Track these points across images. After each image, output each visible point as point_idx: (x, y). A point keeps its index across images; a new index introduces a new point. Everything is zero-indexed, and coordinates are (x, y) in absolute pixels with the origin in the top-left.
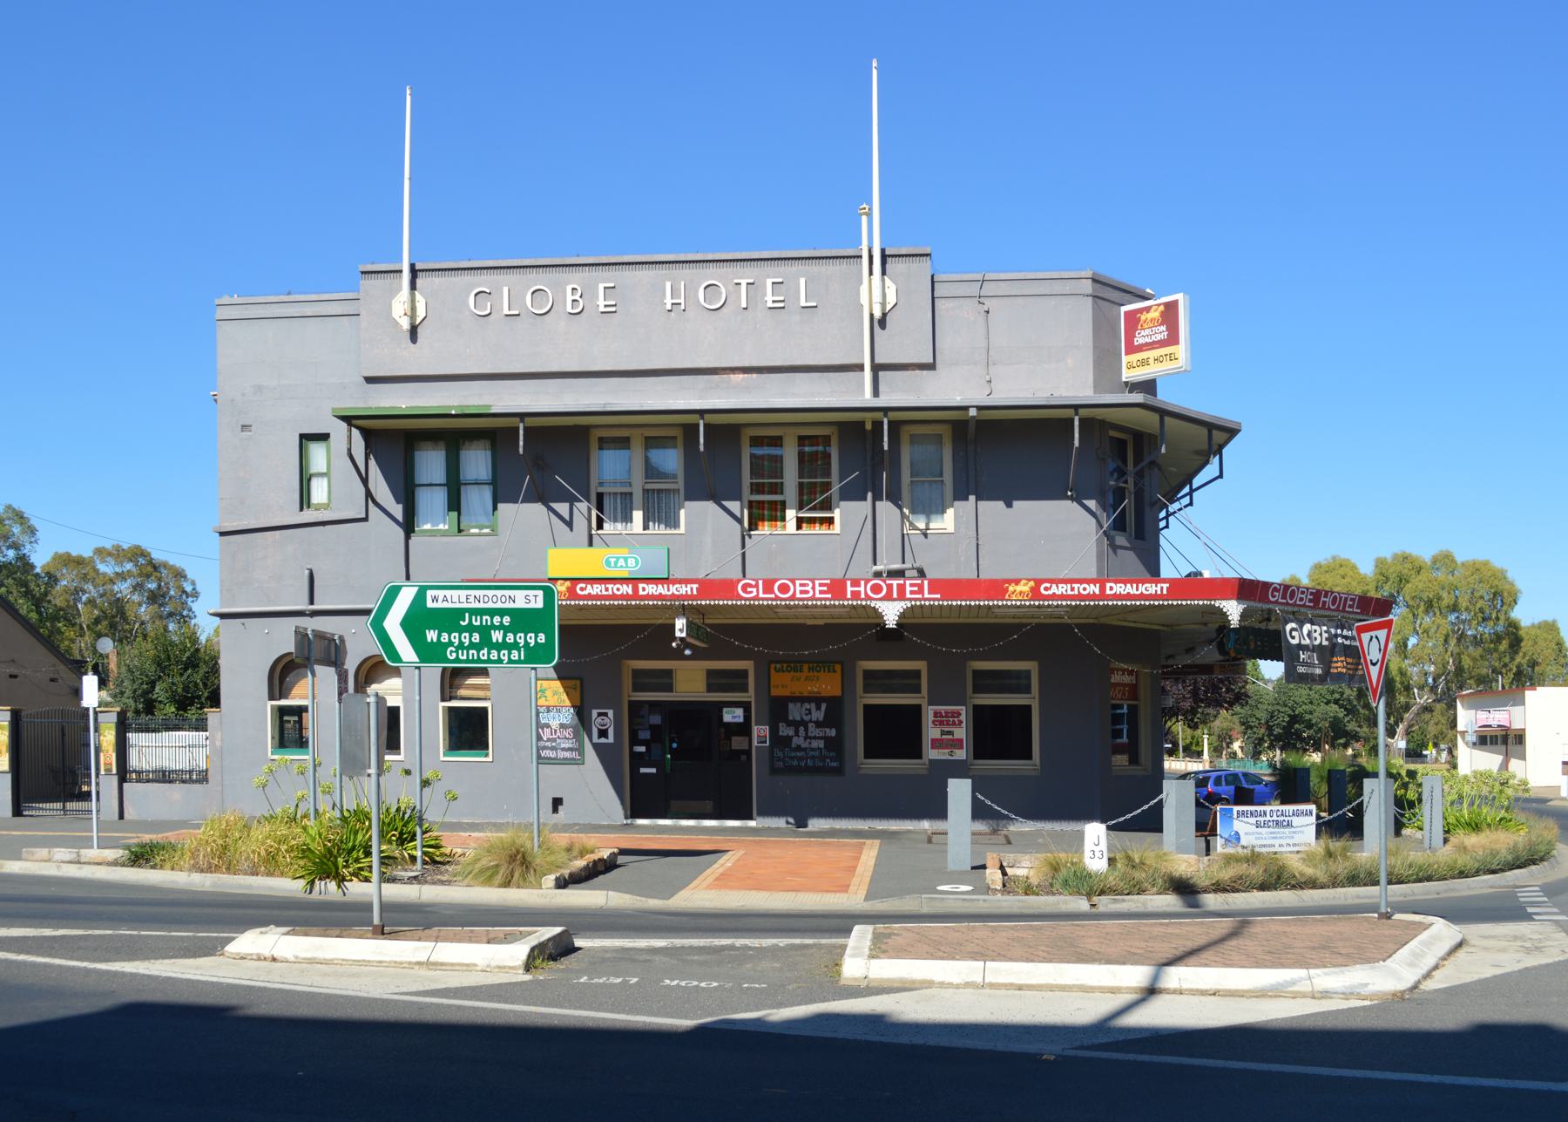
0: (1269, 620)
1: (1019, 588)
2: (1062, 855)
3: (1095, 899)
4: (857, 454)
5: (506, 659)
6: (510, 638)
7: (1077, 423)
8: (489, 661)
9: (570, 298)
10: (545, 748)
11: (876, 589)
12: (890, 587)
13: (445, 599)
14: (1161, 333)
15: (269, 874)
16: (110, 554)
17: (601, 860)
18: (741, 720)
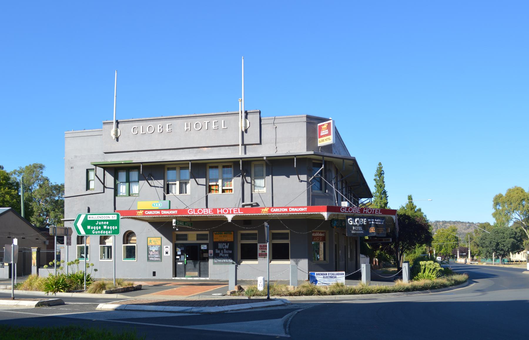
1: (265, 210)
6: (108, 228)
9: (159, 128)
12: (229, 210)
14: (326, 132)
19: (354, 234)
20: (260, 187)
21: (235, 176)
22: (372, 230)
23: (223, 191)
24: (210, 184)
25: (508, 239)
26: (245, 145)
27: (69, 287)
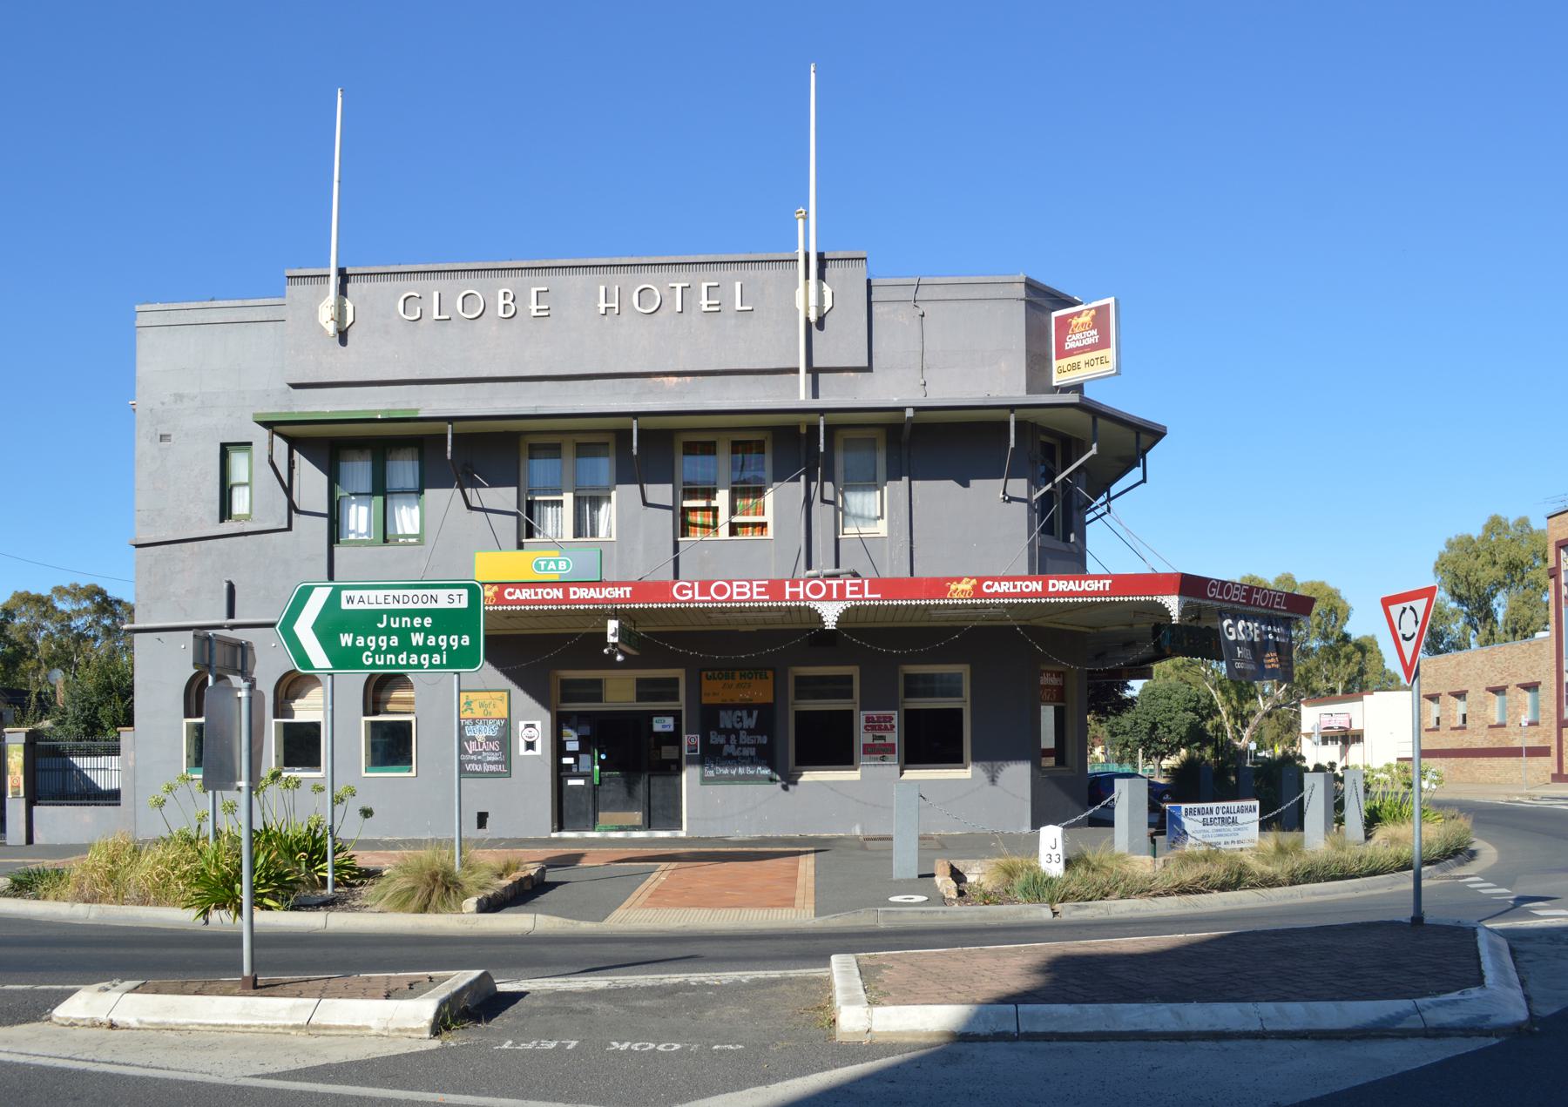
0: (1198, 618)
1: (962, 586)
2: (1016, 859)
3: (1058, 907)
4: (797, 447)
5: (426, 663)
6: (432, 641)
7: (1012, 424)
8: (408, 666)
9: (501, 302)
10: (470, 761)
11: (816, 589)
12: (830, 587)
13: (361, 600)
14: (1092, 337)
15: (158, 903)
16: (68, 593)
17: (529, 877)
18: (671, 729)
20: (862, 517)
21: (779, 476)
23: (734, 529)
24: (687, 504)
25: (1181, 714)
26: (814, 372)
27: (291, 887)
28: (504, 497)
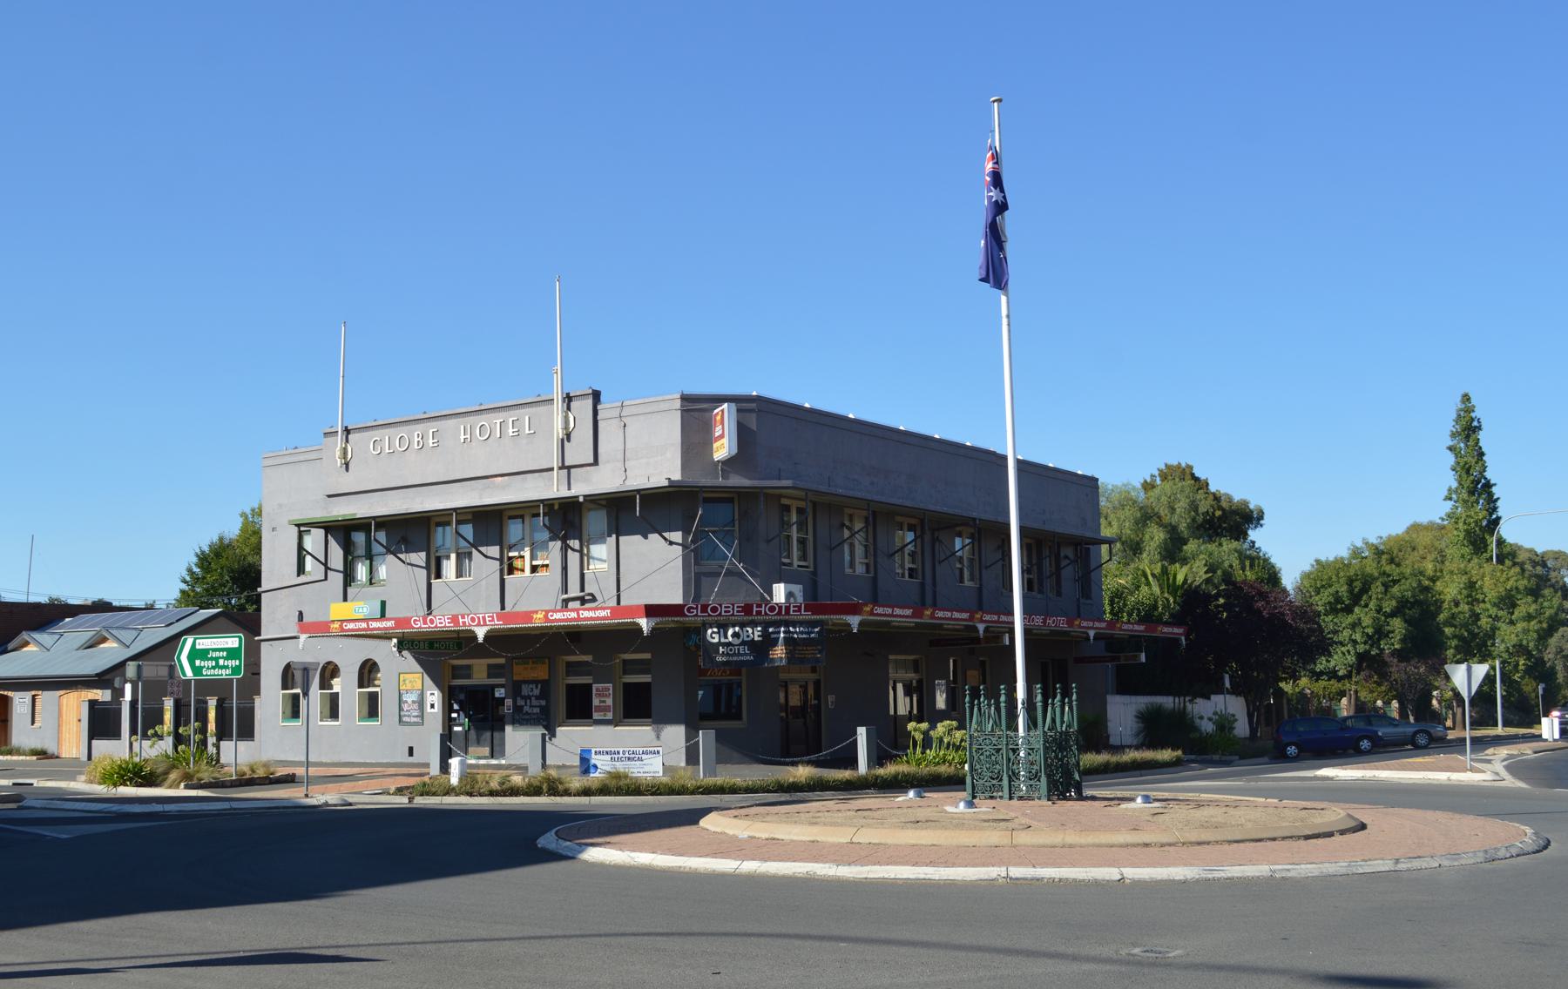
19: (724, 663)
22: (779, 652)
23: (534, 569)
28: (419, 558)
